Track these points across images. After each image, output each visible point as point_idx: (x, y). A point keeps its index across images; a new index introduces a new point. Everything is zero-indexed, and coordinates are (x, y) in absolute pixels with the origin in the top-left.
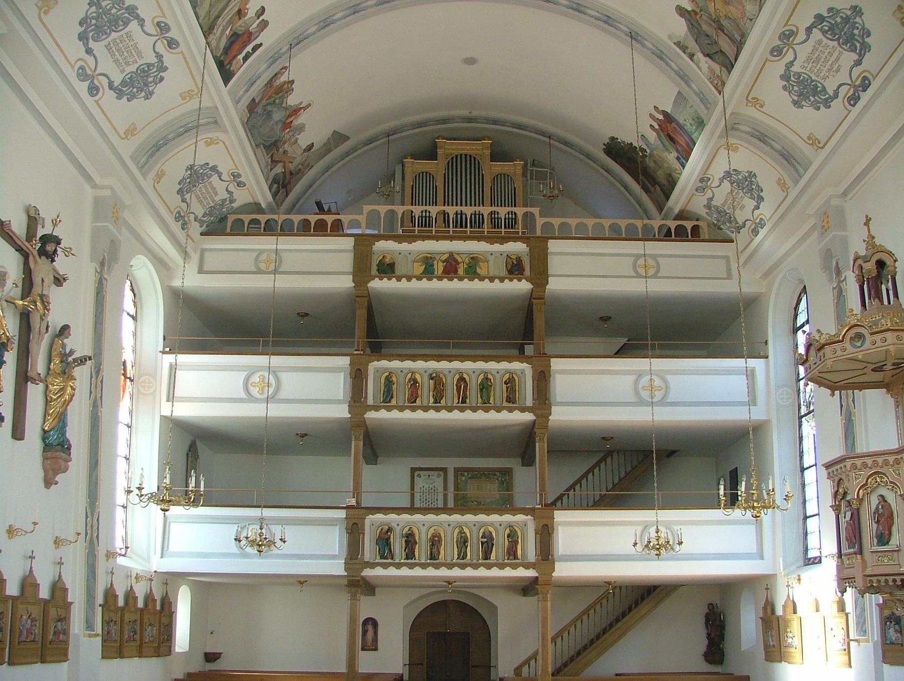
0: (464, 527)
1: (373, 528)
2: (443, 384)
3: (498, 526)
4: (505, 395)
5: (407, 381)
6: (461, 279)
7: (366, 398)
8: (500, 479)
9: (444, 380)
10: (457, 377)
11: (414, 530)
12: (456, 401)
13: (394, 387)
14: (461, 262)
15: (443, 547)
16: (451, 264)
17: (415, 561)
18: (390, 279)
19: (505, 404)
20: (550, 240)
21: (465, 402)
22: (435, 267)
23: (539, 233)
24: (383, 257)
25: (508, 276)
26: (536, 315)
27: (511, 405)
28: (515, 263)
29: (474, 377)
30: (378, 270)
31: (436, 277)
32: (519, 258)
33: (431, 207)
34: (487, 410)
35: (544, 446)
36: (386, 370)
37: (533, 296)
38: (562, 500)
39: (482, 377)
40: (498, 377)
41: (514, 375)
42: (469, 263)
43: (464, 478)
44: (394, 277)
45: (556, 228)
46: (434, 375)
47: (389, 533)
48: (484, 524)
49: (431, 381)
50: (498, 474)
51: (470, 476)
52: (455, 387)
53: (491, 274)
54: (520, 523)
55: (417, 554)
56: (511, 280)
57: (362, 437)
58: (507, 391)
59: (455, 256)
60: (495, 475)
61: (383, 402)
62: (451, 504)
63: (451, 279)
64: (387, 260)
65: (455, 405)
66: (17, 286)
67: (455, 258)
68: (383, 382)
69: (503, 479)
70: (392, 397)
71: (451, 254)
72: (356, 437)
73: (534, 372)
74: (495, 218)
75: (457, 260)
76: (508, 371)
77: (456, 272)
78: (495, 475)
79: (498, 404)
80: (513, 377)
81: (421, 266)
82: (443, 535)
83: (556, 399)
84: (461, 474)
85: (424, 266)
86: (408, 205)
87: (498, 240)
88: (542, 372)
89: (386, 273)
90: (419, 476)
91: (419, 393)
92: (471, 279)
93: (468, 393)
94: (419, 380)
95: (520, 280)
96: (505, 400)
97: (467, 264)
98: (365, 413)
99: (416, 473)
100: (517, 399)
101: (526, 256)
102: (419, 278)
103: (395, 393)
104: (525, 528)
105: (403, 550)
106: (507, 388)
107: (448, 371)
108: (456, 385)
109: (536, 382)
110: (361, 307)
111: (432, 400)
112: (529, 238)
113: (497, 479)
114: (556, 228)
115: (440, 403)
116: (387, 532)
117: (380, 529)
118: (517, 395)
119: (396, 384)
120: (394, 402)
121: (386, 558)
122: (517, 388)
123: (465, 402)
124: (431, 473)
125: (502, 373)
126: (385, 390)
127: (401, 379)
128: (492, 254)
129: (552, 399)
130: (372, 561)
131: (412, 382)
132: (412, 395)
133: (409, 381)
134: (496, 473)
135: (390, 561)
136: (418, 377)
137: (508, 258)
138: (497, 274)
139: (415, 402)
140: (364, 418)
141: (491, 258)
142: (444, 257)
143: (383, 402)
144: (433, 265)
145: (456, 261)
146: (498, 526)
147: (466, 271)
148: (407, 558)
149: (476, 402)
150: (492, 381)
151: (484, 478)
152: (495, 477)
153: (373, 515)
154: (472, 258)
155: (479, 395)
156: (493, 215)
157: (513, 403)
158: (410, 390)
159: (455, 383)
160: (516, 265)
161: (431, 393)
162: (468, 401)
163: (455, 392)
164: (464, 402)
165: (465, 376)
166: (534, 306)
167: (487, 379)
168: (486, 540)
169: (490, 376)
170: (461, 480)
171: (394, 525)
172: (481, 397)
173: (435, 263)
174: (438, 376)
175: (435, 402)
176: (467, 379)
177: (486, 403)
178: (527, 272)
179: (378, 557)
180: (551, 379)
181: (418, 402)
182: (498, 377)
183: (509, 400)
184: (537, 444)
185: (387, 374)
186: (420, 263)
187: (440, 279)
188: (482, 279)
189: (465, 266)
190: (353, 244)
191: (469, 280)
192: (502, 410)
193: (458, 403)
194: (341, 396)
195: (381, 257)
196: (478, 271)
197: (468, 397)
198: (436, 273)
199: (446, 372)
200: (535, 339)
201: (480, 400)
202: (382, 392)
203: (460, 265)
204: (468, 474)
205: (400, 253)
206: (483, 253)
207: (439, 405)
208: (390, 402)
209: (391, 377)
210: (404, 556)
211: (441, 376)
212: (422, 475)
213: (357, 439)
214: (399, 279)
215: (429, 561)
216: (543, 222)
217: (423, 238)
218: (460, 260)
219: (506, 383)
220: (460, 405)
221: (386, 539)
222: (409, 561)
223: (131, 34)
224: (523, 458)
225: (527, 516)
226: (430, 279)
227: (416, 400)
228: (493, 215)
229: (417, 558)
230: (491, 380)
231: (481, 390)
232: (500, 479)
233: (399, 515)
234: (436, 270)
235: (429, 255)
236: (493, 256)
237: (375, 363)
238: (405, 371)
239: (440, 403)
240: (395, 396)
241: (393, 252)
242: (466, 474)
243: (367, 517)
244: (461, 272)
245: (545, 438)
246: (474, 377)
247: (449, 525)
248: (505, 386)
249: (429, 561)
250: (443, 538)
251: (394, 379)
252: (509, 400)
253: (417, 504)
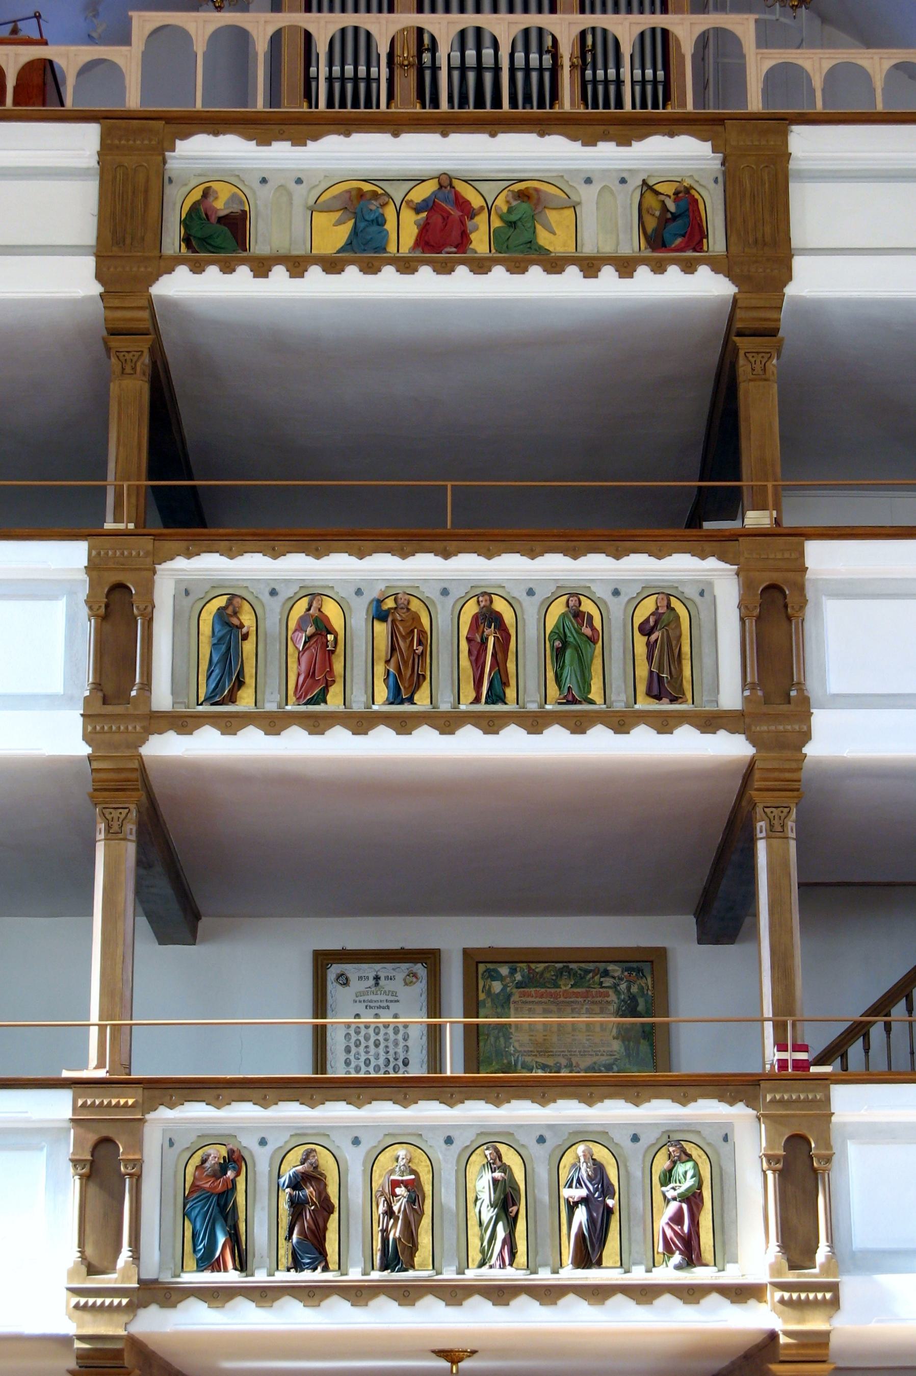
0: (503, 1149)
1: (172, 1153)
2: (422, 632)
3: (626, 1143)
4: (643, 671)
5: (292, 624)
6: (481, 266)
7: (147, 685)
8: (623, 986)
9: (425, 621)
10: (471, 609)
11: (322, 1162)
12: (468, 692)
13: (248, 647)
14: (482, 208)
15: (426, 1222)
16: (446, 217)
17: (328, 1276)
18: (228, 268)
19: (644, 704)
20: (795, 128)
21: (502, 700)
22: (390, 226)
23: (755, 103)
24: (206, 193)
25: (648, 253)
26: (748, 391)
27: (665, 706)
28: (672, 207)
29: (531, 609)
30: (187, 240)
31: (394, 261)
32: (688, 190)
33: (374, 16)
34: (578, 725)
35: (788, 850)
36: (216, 587)
37: (738, 325)
38: (866, 1036)
39: (558, 609)
40: (617, 608)
41: (675, 603)
42: (510, 210)
43: (497, 986)
44: (243, 261)
45: (818, 83)
46: (390, 604)
47: (230, 1174)
48: (581, 1135)
49: (382, 629)
50: (615, 969)
51: (518, 977)
52: (464, 646)
53: (588, 249)
54: (706, 1132)
55: (331, 1246)
56: (659, 268)
57: (131, 827)
58: (650, 658)
59: (461, 187)
60: (606, 973)
61: (210, 699)
62: (452, 1067)
63: (445, 268)
64: (221, 205)
65: (463, 707)
66: (265, 1096)
67: (457, 195)
68: (206, 628)
69: (634, 989)
70: (240, 683)
71: (446, 182)
72: (108, 828)
73: (747, 586)
74: (595, 81)
75: (467, 203)
76: (649, 589)
77: (463, 243)
78: (606, 973)
79: (619, 701)
80: (669, 606)
81: (339, 223)
82: (426, 1179)
83: (823, 681)
84: (488, 970)
85: (351, 224)
86: (291, 10)
87: (612, 129)
88: (773, 588)
89: (217, 249)
90: (343, 979)
91: (338, 667)
92: (518, 267)
93: (511, 666)
94: (336, 622)
95: (689, 268)
96: (642, 688)
97: (501, 217)
98: (144, 741)
99: (333, 971)
100: (687, 686)
101: (712, 185)
102: (333, 265)
103: (249, 671)
104: (724, 1148)
105: (283, 1233)
106: (650, 647)
107: (439, 587)
108: (469, 640)
109: (750, 624)
110: (128, 370)
111: (382, 692)
112: (719, 121)
113: (615, 987)
114: (818, 83)
115: (411, 700)
116: (223, 1168)
117: (196, 1160)
118: (687, 672)
119: (252, 638)
120: (245, 702)
121: (217, 1266)
122: (686, 649)
123: (502, 700)
124: (383, 969)
125: (629, 592)
126: (215, 659)
127: (272, 622)
128: (588, 181)
129: (813, 686)
130: (166, 1278)
131: (310, 630)
132: (311, 674)
133: (300, 628)
134: (611, 967)
135: (231, 1276)
136: (332, 611)
137: (649, 196)
138: (607, 249)
139: (321, 698)
140: (140, 756)
141: (587, 196)
142: (421, 193)
143: (210, 699)
144: (380, 221)
145: (468, 211)
146: (626, 1143)
147: (499, 240)
148: (297, 1265)
149: (538, 697)
150: (597, 623)
151: (566, 985)
152: (608, 982)
153: (171, 1107)
154: (523, 196)
155: (551, 675)
156: (589, 73)
157: (673, 700)
158: (304, 660)
159: (464, 631)
160: (675, 217)
161: (380, 669)
162: (510, 693)
163: (465, 662)
164: (496, 697)
165: (500, 606)
166: (742, 361)
167: (578, 615)
168: (583, 1192)
169: (588, 607)
170: (489, 993)
171: (248, 1142)
172: (558, 679)
173: (390, 213)
174: (403, 606)
175: (396, 697)
176: (508, 617)
177: (575, 702)
178: (716, 242)
179: (190, 1262)
180: (809, 610)
181: (334, 702)
182: (617, 608)
183: (657, 690)
184: (761, 847)
185: (221, 602)
186: (337, 215)
187: (406, 266)
188: (554, 265)
189: (497, 223)
190: (97, 147)
191: (510, 270)
192: (636, 724)
193: (477, 700)
194: (57, 686)
195: (197, 195)
196: (543, 238)
197: (513, 682)
198: (392, 248)
199: (432, 593)
200: (744, 476)
201: (553, 690)
202: (204, 666)
203: (477, 219)
204: (513, 971)
205: (264, 181)
206: (558, 180)
207: (406, 708)
208: (231, 699)
209: (235, 614)
210: (285, 1259)
211: (415, 605)
212: (353, 978)
213: (113, 834)
214: (261, 268)
215: (376, 1275)
216: (772, 63)
217: (347, 126)
218: (476, 201)
219: (646, 629)
220: (482, 707)
221: (220, 1195)
222: (307, 1276)
223: (355, 998)
224: (702, 912)
225: (732, 1104)
226: (370, 268)
227: (325, 691)
228: (589, 73)
229: (333, 1265)
230: (590, 617)
231: (559, 654)
232: (623, 986)
233: (265, 1107)
234: (393, 236)
235: (367, 187)
236: (595, 188)
237: (180, 563)
238: (286, 593)
239: (411, 700)
240: (249, 680)
241: (233, 177)
242: (504, 970)
243: (150, 1116)
244: (480, 243)
245: (791, 824)
246: (531, 609)
247: (449, 1141)
248: (641, 642)
249: (376, 1275)
250: (427, 1189)
251: (247, 619)
252: (657, 690)
253: (337, 1070)
